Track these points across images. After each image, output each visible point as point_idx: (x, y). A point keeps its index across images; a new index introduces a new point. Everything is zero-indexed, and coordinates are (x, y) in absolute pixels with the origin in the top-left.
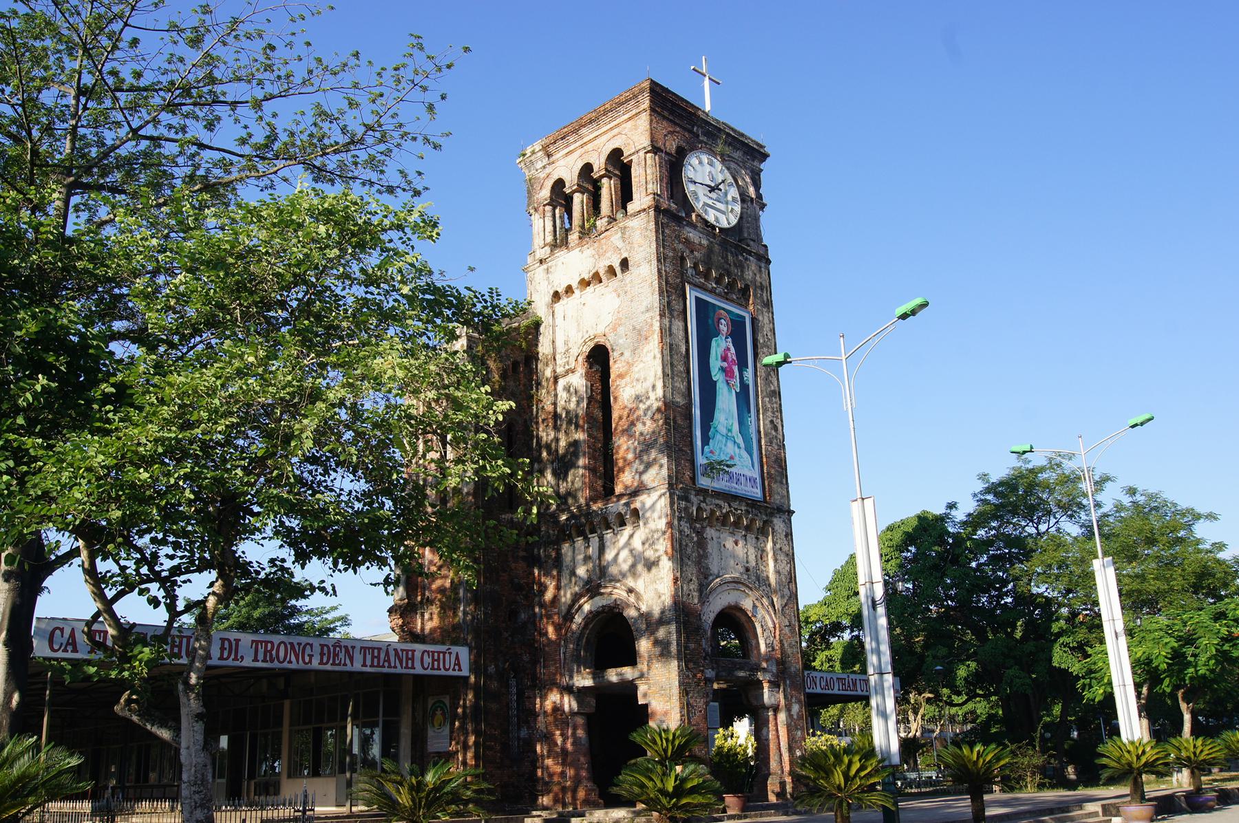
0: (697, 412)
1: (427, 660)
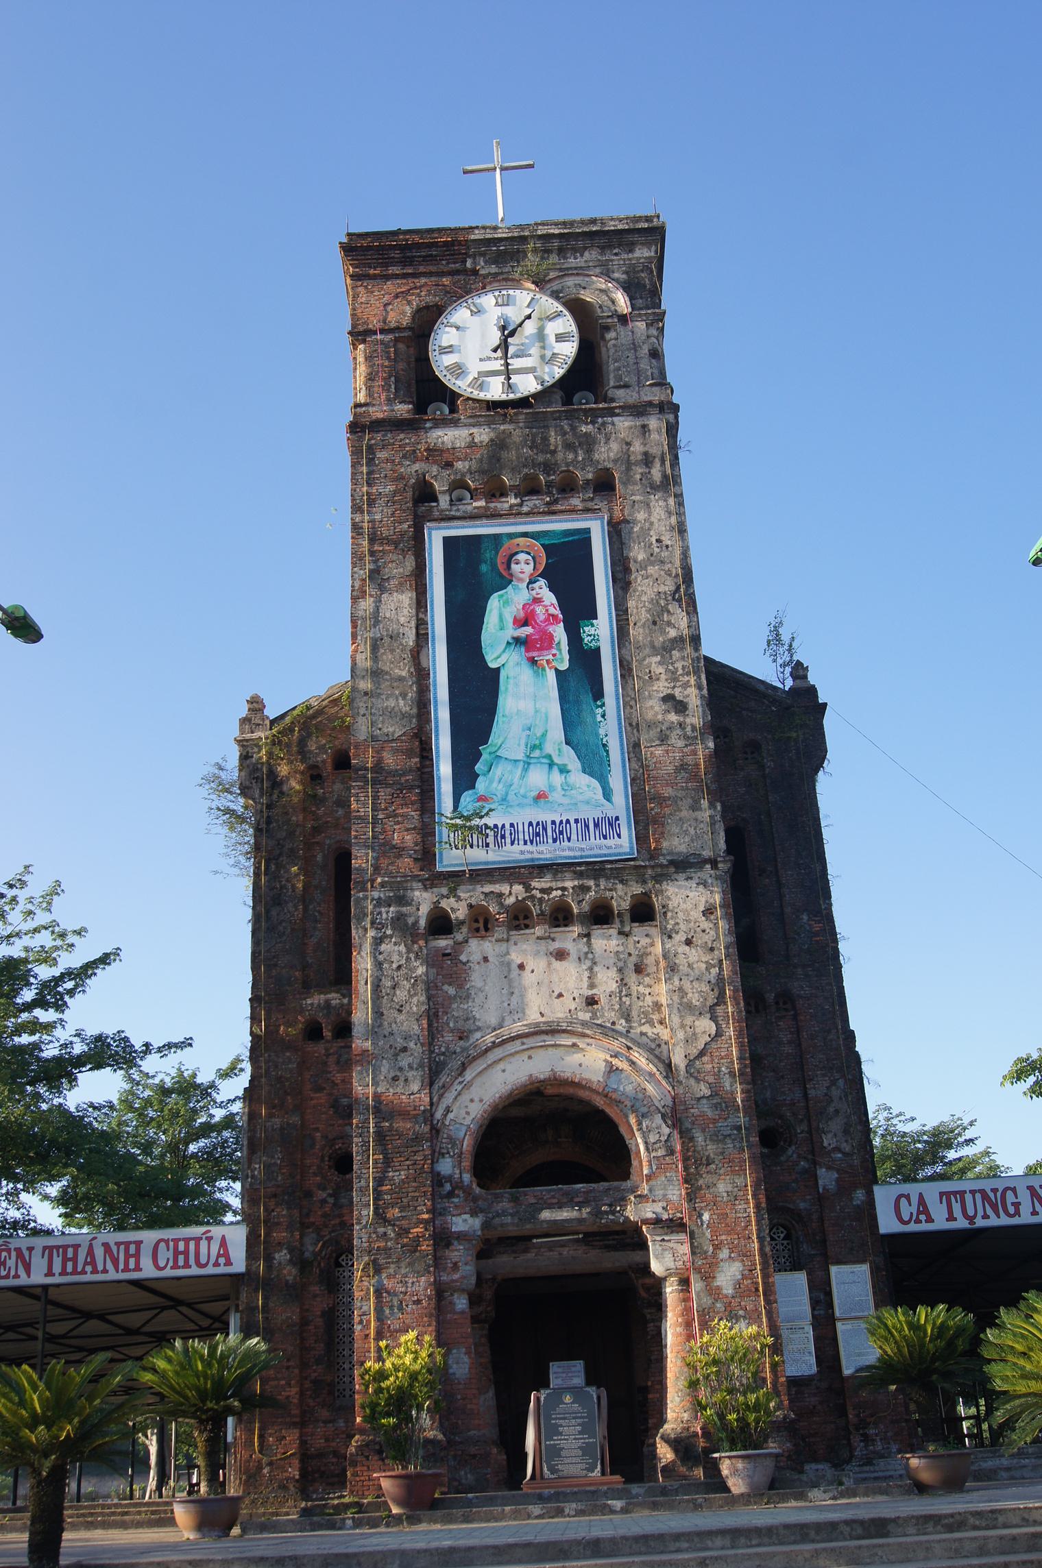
0: (443, 744)
1: (164, 1255)
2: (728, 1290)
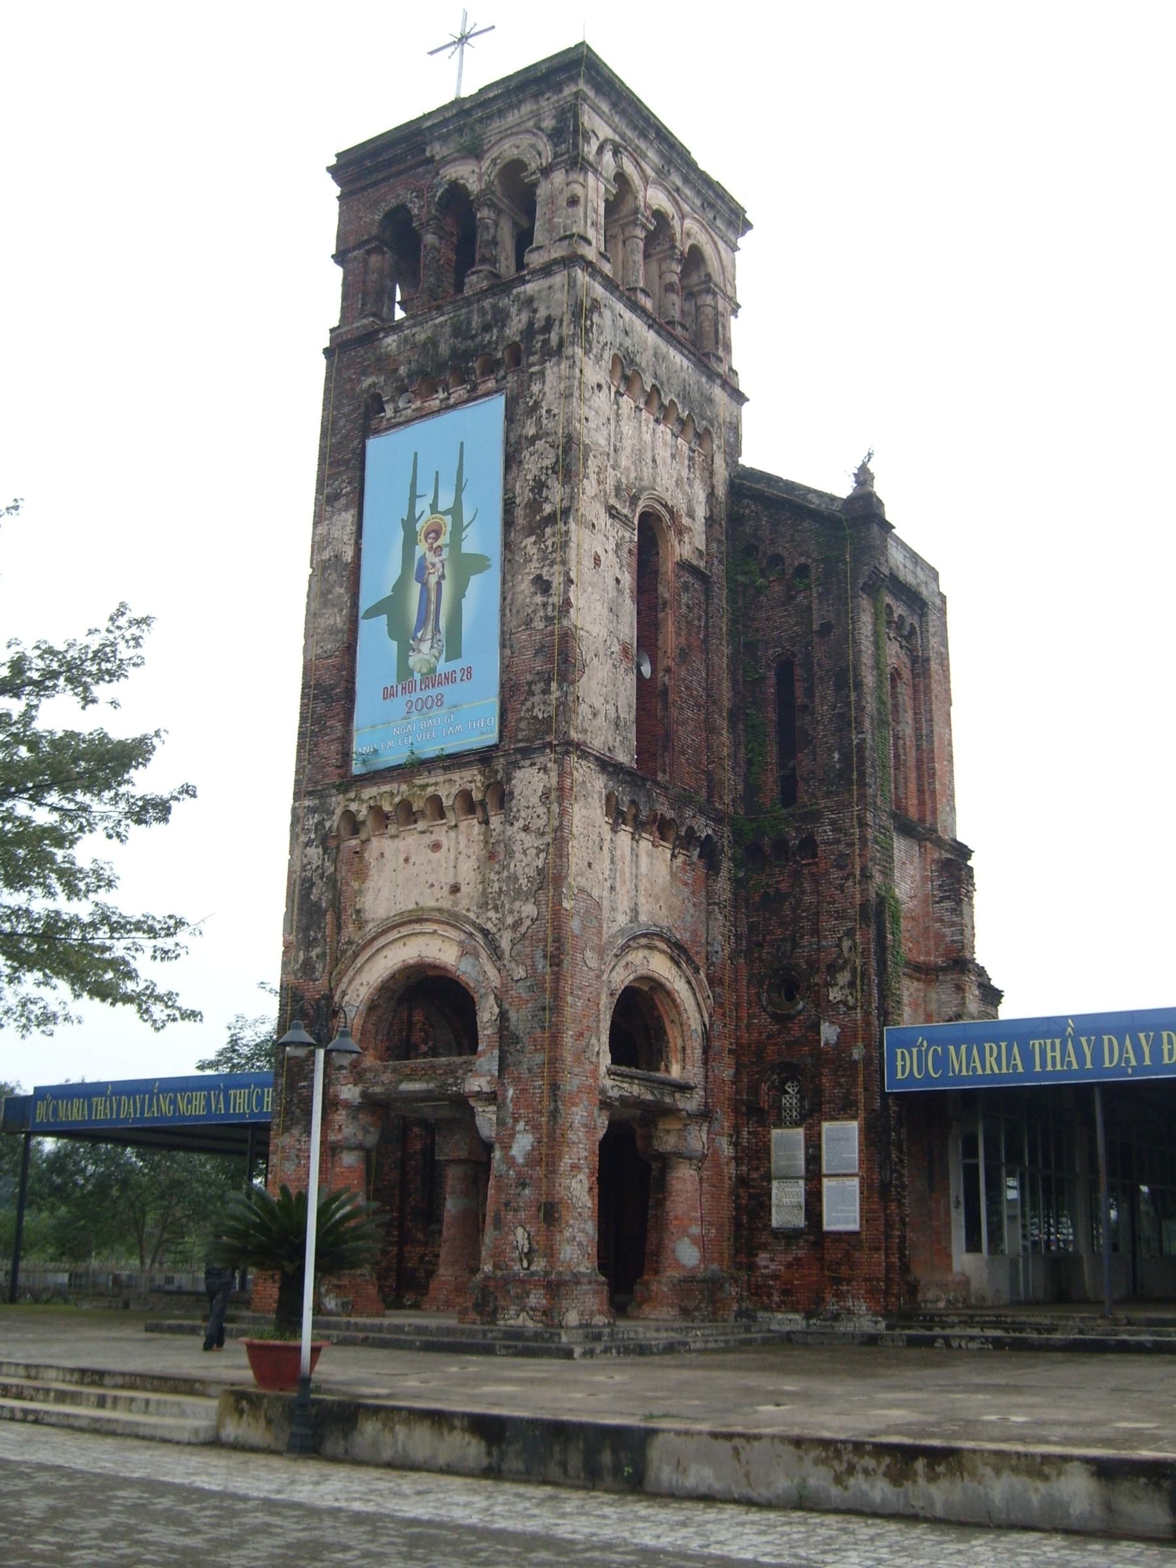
2: (520, 1160)
